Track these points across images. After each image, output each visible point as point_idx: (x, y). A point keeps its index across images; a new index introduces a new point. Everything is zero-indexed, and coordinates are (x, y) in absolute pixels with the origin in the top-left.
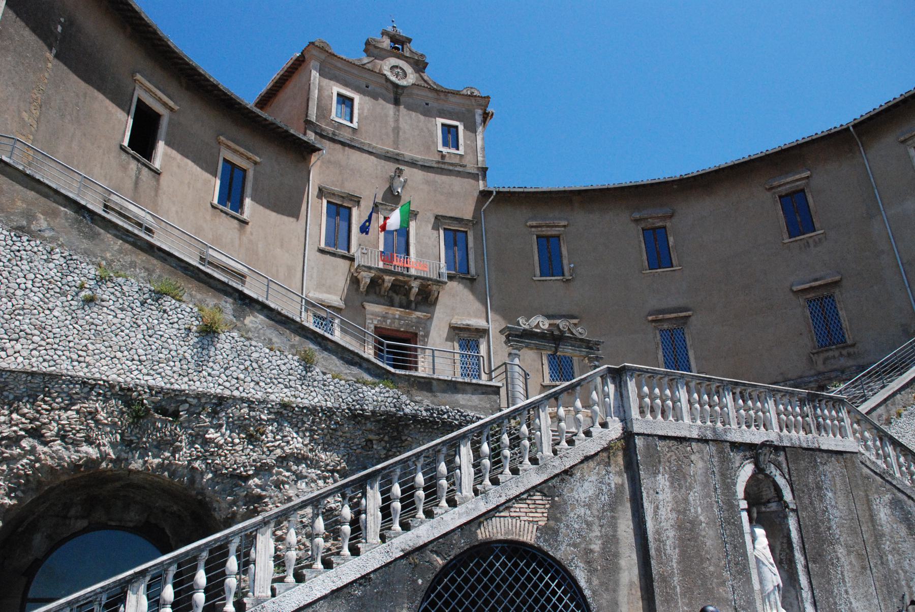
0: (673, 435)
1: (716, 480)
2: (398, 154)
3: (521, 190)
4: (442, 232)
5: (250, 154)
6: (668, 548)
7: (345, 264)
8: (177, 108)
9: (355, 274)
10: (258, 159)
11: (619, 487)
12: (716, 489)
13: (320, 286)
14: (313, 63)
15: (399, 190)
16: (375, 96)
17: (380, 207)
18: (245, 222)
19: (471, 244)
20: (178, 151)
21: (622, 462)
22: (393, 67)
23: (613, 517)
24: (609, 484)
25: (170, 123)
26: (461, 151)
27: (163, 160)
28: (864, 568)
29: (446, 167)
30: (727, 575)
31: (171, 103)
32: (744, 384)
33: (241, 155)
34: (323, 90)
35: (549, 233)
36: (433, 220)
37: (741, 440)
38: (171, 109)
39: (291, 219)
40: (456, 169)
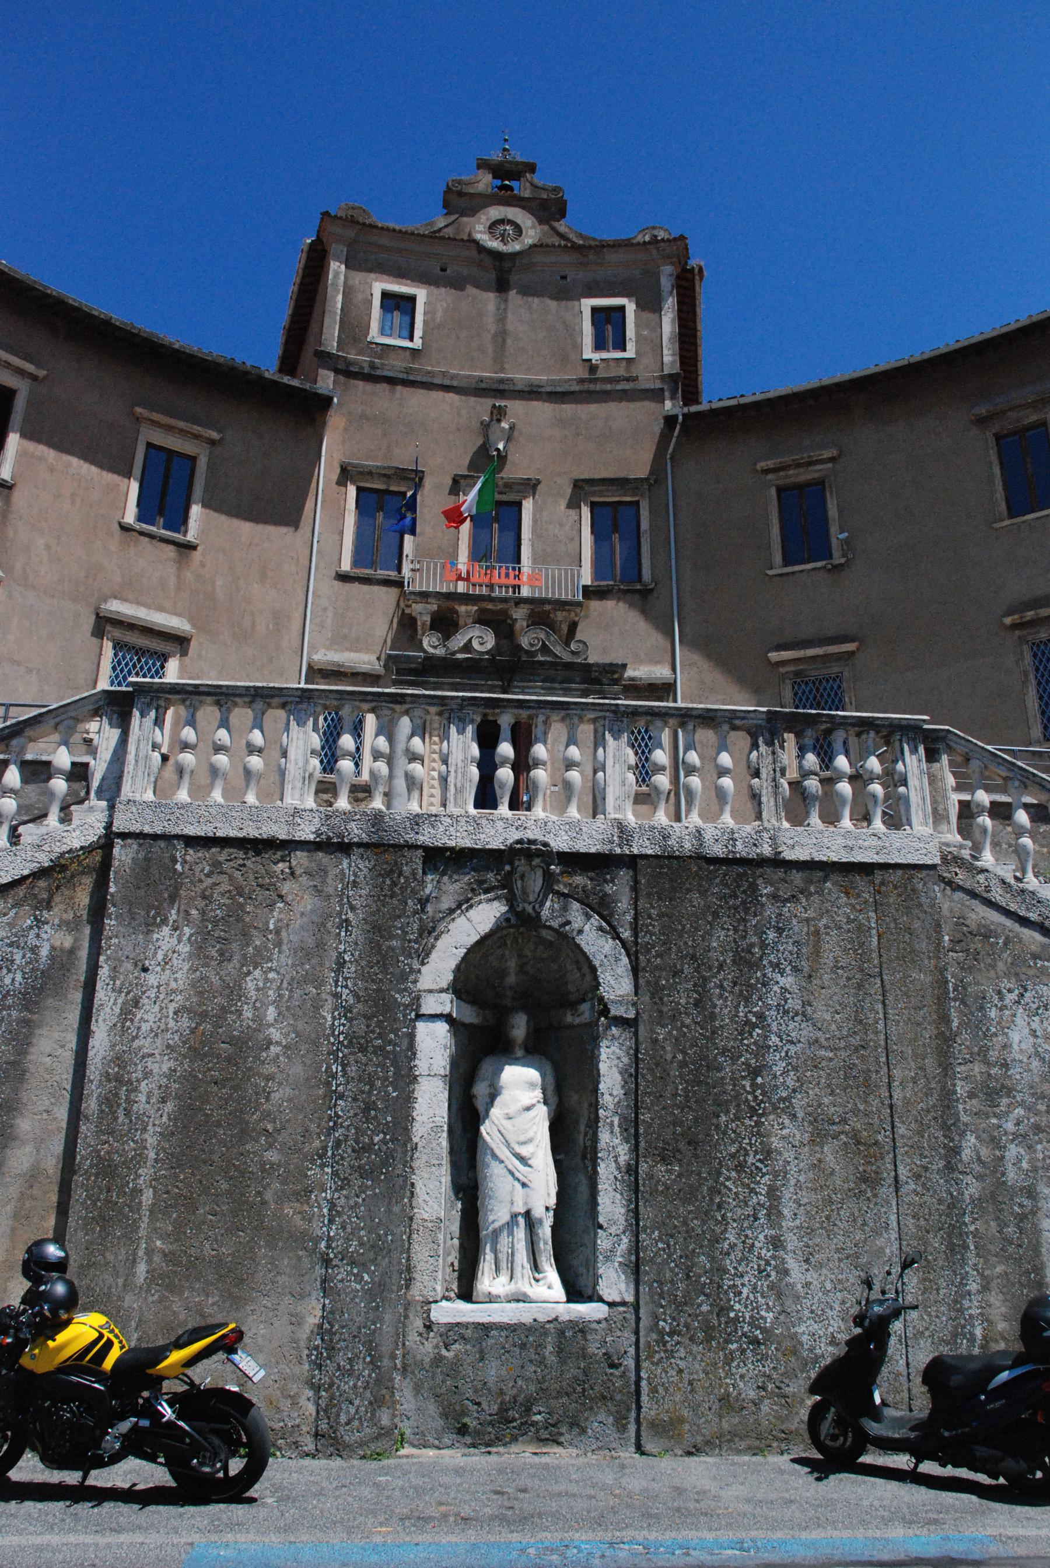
0: (233, 833)
1: (348, 945)
2: (502, 381)
3: (733, 402)
4: (586, 512)
5: (197, 429)
6: (142, 1098)
7: (387, 596)
8: (42, 373)
9: (407, 611)
10: (215, 435)
11: (62, 960)
12: (341, 964)
13: (338, 641)
14: (337, 248)
15: (501, 446)
16: (457, 284)
17: (462, 481)
18: (191, 547)
19: (645, 525)
20: (50, 445)
21: (86, 901)
22: (493, 226)
23: (26, 1022)
24: (35, 950)
25: (30, 403)
26: (630, 353)
27: (17, 462)
28: (869, 1180)
29: (599, 387)
30: (321, 1174)
31: (30, 368)
32: (521, 704)
33: (183, 432)
34: (359, 293)
35: (802, 478)
36: (569, 491)
37: (468, 843)
38: (34, 378)
39: (284, 530)
40: (619, 387)
